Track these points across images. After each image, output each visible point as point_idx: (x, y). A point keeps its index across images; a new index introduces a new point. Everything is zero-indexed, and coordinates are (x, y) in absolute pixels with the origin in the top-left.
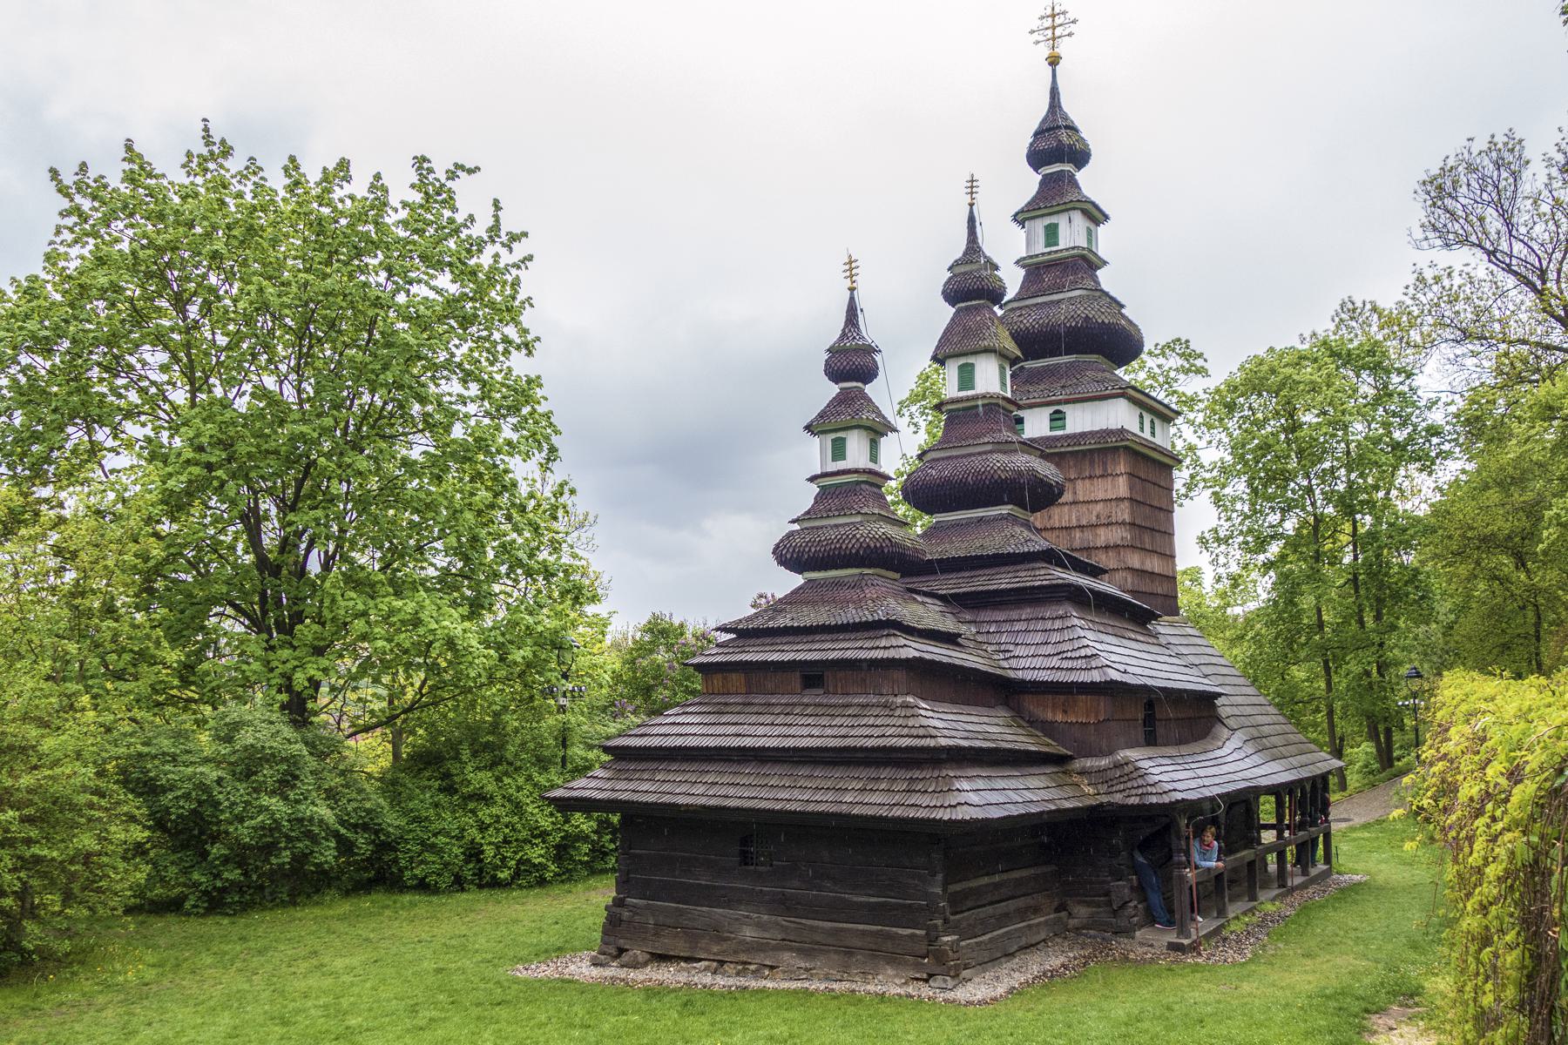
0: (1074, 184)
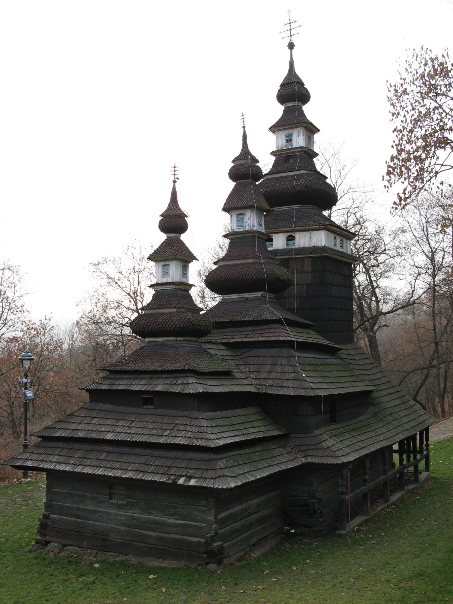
0: (302, 114)
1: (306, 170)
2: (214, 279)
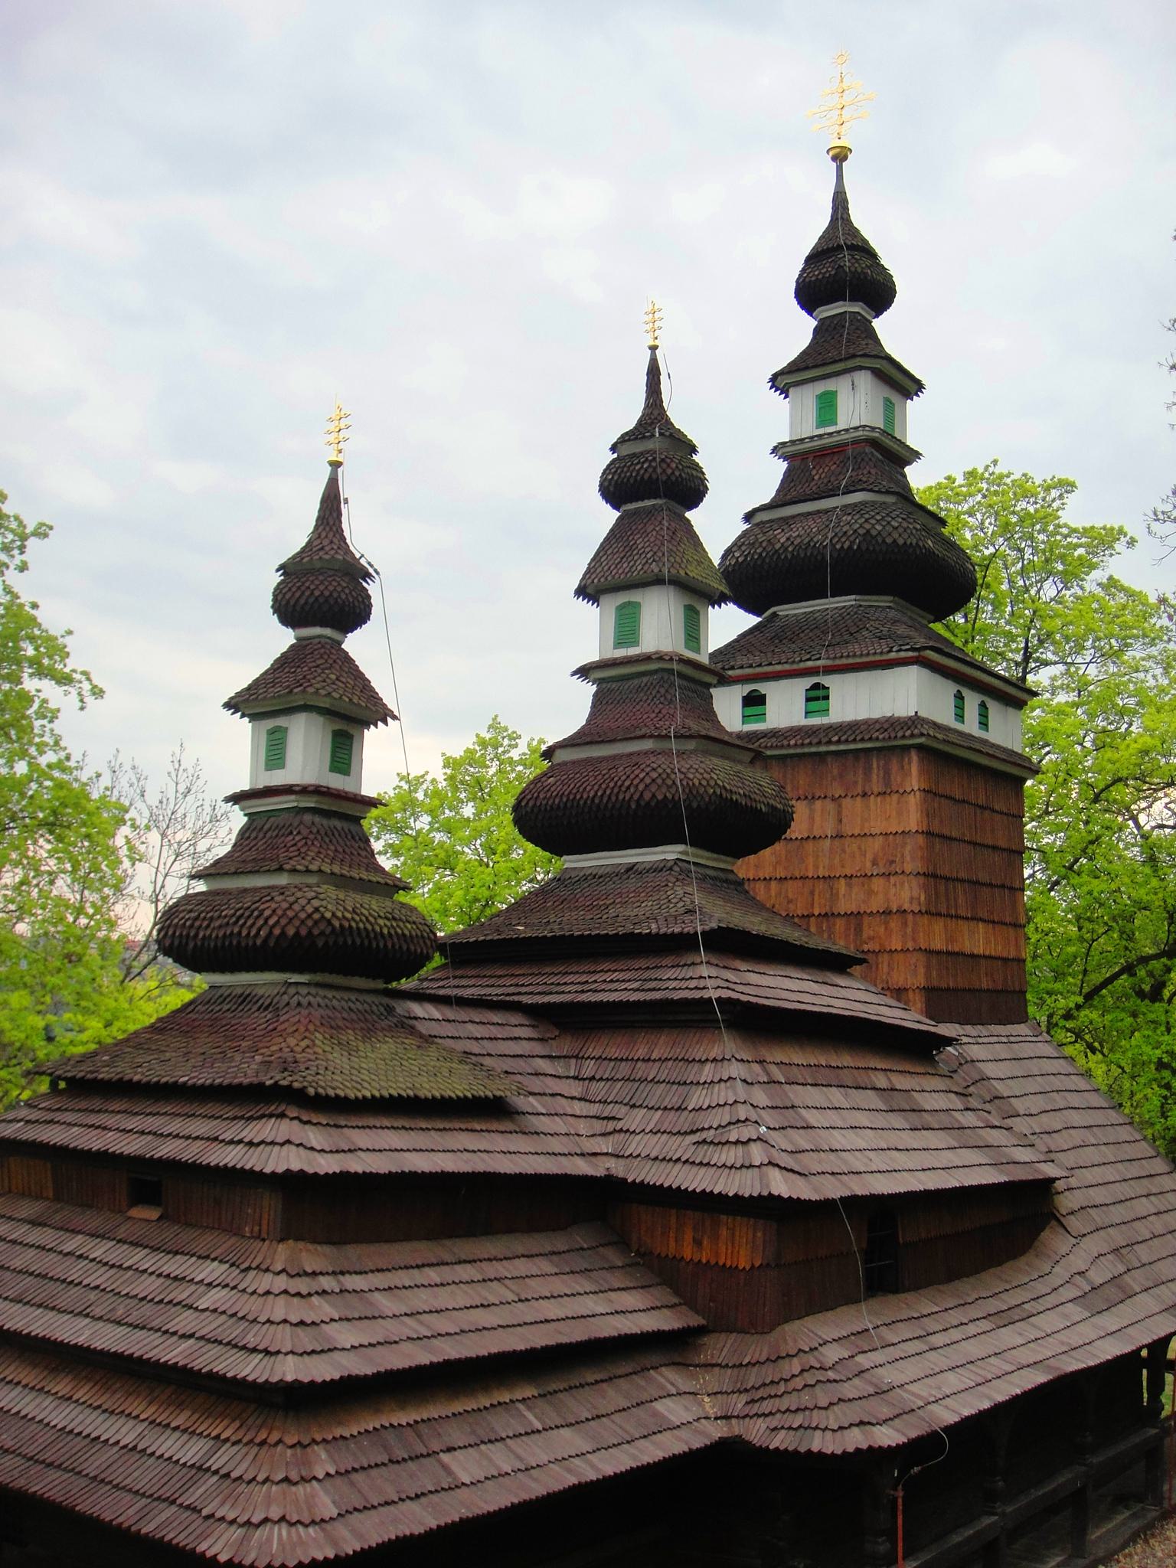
0: (872, 335)
1: (871, 490)
2: (531, 804)
